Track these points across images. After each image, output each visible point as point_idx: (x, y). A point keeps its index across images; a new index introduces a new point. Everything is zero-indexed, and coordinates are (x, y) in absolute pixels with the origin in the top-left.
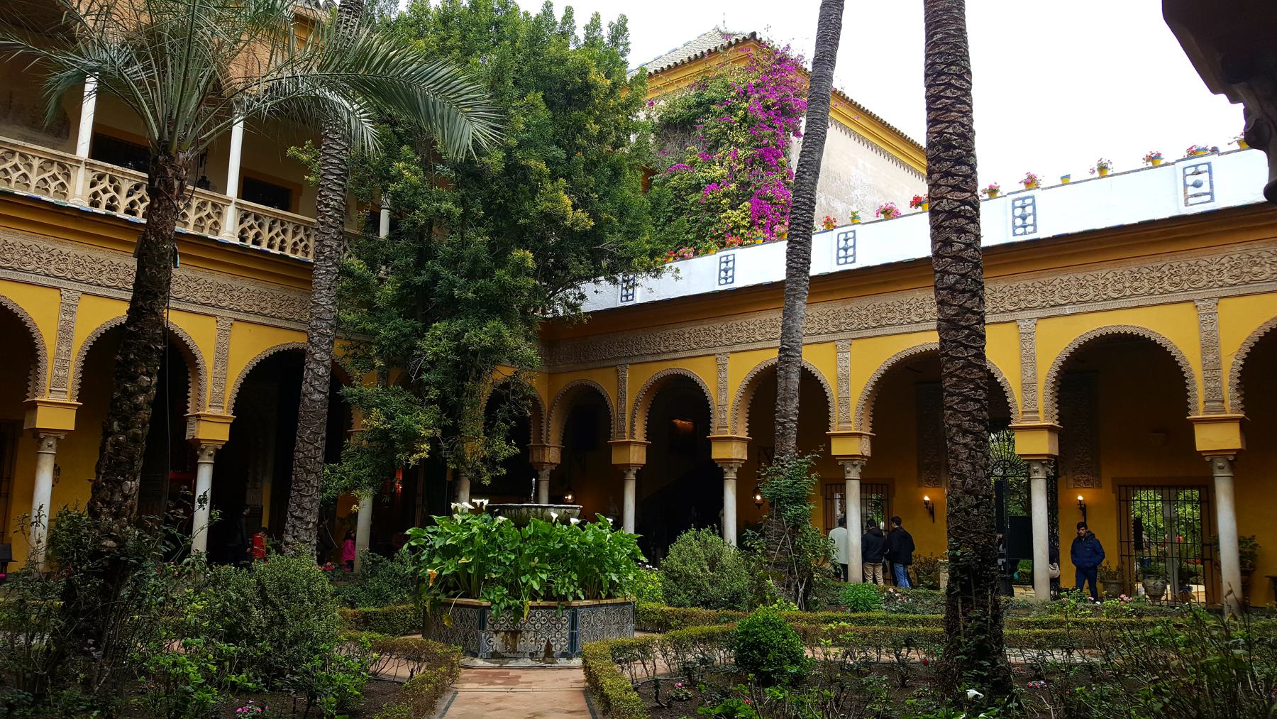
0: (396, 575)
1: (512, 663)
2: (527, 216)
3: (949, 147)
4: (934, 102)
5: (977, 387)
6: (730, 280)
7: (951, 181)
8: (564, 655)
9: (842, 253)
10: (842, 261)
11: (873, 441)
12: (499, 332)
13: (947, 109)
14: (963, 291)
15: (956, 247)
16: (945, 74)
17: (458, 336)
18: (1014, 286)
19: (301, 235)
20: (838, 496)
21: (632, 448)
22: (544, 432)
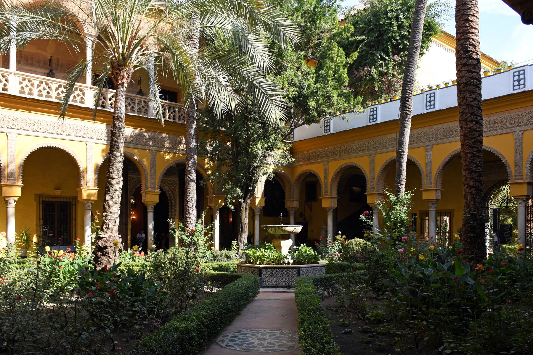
6: (375, 120)
9: (428, 104)
10: (428, 108)
18: (512, 115)
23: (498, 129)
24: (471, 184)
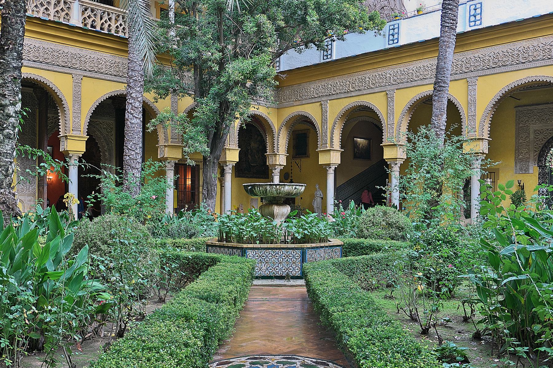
9: (472, 19)
19: (121, 21)
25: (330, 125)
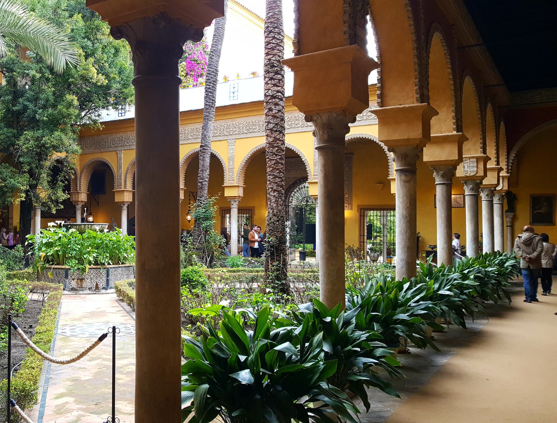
0: (16, 257)
1: (81, 292)
2: (73, 77)
3: (273, 66)
4: (267, 45)
5: (280, 172)
7: (273, 82)
8: (104, 288)
11: (245, 189)
12: (61, 138)
13: (273, 49)
14: (276, 131)
15: (274, 112)
16: (272, 32)
17: (38, 139)
20: (228, 215)
21: (125, 193)
22: (78, 185)
23: (299, 127)
24: (275, 188)
25: (123, 170)
